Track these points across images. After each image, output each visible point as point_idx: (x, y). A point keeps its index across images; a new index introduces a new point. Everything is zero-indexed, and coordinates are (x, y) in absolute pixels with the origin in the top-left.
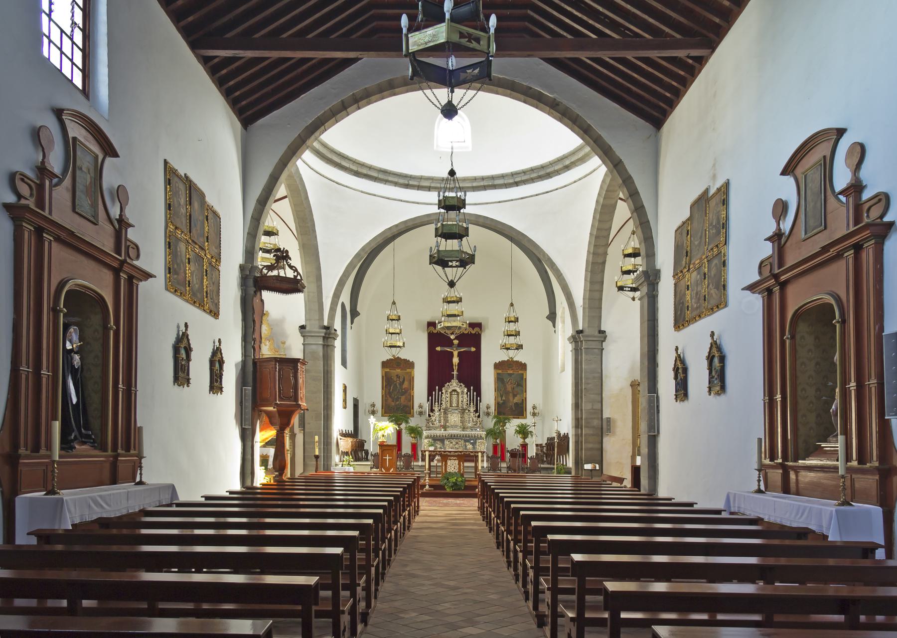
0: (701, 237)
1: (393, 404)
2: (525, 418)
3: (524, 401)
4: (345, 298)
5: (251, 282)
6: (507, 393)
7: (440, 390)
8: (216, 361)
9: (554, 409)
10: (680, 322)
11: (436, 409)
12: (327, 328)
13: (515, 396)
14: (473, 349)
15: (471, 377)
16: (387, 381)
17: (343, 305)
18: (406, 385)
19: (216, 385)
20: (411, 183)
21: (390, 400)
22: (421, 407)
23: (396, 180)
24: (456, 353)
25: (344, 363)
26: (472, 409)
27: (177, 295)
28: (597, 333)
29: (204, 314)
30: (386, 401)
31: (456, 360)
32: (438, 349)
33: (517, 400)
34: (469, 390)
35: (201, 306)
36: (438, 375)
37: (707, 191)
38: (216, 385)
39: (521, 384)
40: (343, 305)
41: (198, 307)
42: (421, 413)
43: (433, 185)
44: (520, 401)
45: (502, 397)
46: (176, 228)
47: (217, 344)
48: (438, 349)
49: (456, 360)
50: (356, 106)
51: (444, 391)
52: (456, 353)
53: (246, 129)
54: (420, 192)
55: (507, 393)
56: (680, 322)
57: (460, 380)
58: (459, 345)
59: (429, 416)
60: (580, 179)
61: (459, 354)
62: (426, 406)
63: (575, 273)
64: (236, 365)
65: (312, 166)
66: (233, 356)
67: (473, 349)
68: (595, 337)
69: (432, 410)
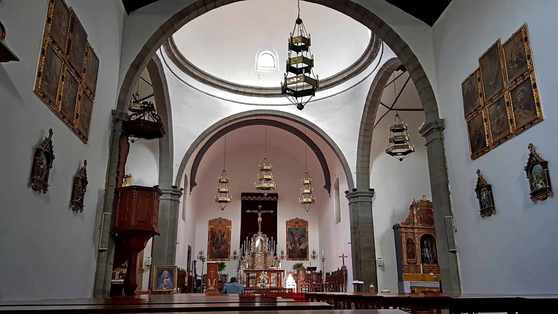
0: (497, 77)
1: (216, 251)
2: (308, 260)
3: (307, 247)
4: (187, 171)
5: (120, 125)
6: (295, 242)
7: (250, 239)
8: (80, 181)
9: (332, 247)
10: (478, 147)
11: (246, 253)
12: (175, 187)
13: (300, 244)
14: (272, 212)
15: (271, 231)
16: (213, 235)
17: (186, 175)
18: (225, 237)
19: (77, 203)
20: (239, 90)
21: (214, 248)
22: (235, 253)
23: (229, 87)
24: (260, 214)
25: (184, 218)
26: (272, 253)
27: (44, 102)
28: (367, 191)
29: (72, 133)
30: (210, 249)
31: (260, 219)
32: (248, 211)
33: (303, 247)
34: (270, 239)
35: (70, 124)
36: (248, 232)
37: (499, 41)
38: (77, 203)
39: (304, 236)
40: (186, 175)
41: (67, 124)
42: (235, 258)
43: (254, 92)
44: (304, 248)
45: (291, 245)
46: (54, 42)
47: (83, 165)
48: (248, 211)
49: (260, 219)
50: (213, 3)
51: (252, 240)
52: (260, 214)
53: (128, 14)
54: (245, 96)
55: (295, 242)
56: (478, 147)
57: (264, 232)
58: (262, 209)
59: (242, 259)
60: (355, 86)
61: (263, 215)
62: (239, 254)
63: (350, 151)
64: (99, 191)
65: (173, 71)
66: (97, 182)
67: (272, 212)
68: (366, 193)
69: (244, 255)
